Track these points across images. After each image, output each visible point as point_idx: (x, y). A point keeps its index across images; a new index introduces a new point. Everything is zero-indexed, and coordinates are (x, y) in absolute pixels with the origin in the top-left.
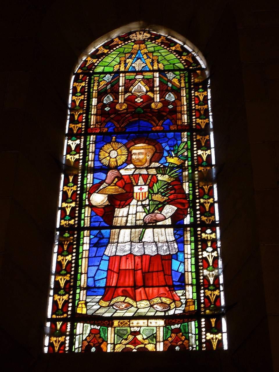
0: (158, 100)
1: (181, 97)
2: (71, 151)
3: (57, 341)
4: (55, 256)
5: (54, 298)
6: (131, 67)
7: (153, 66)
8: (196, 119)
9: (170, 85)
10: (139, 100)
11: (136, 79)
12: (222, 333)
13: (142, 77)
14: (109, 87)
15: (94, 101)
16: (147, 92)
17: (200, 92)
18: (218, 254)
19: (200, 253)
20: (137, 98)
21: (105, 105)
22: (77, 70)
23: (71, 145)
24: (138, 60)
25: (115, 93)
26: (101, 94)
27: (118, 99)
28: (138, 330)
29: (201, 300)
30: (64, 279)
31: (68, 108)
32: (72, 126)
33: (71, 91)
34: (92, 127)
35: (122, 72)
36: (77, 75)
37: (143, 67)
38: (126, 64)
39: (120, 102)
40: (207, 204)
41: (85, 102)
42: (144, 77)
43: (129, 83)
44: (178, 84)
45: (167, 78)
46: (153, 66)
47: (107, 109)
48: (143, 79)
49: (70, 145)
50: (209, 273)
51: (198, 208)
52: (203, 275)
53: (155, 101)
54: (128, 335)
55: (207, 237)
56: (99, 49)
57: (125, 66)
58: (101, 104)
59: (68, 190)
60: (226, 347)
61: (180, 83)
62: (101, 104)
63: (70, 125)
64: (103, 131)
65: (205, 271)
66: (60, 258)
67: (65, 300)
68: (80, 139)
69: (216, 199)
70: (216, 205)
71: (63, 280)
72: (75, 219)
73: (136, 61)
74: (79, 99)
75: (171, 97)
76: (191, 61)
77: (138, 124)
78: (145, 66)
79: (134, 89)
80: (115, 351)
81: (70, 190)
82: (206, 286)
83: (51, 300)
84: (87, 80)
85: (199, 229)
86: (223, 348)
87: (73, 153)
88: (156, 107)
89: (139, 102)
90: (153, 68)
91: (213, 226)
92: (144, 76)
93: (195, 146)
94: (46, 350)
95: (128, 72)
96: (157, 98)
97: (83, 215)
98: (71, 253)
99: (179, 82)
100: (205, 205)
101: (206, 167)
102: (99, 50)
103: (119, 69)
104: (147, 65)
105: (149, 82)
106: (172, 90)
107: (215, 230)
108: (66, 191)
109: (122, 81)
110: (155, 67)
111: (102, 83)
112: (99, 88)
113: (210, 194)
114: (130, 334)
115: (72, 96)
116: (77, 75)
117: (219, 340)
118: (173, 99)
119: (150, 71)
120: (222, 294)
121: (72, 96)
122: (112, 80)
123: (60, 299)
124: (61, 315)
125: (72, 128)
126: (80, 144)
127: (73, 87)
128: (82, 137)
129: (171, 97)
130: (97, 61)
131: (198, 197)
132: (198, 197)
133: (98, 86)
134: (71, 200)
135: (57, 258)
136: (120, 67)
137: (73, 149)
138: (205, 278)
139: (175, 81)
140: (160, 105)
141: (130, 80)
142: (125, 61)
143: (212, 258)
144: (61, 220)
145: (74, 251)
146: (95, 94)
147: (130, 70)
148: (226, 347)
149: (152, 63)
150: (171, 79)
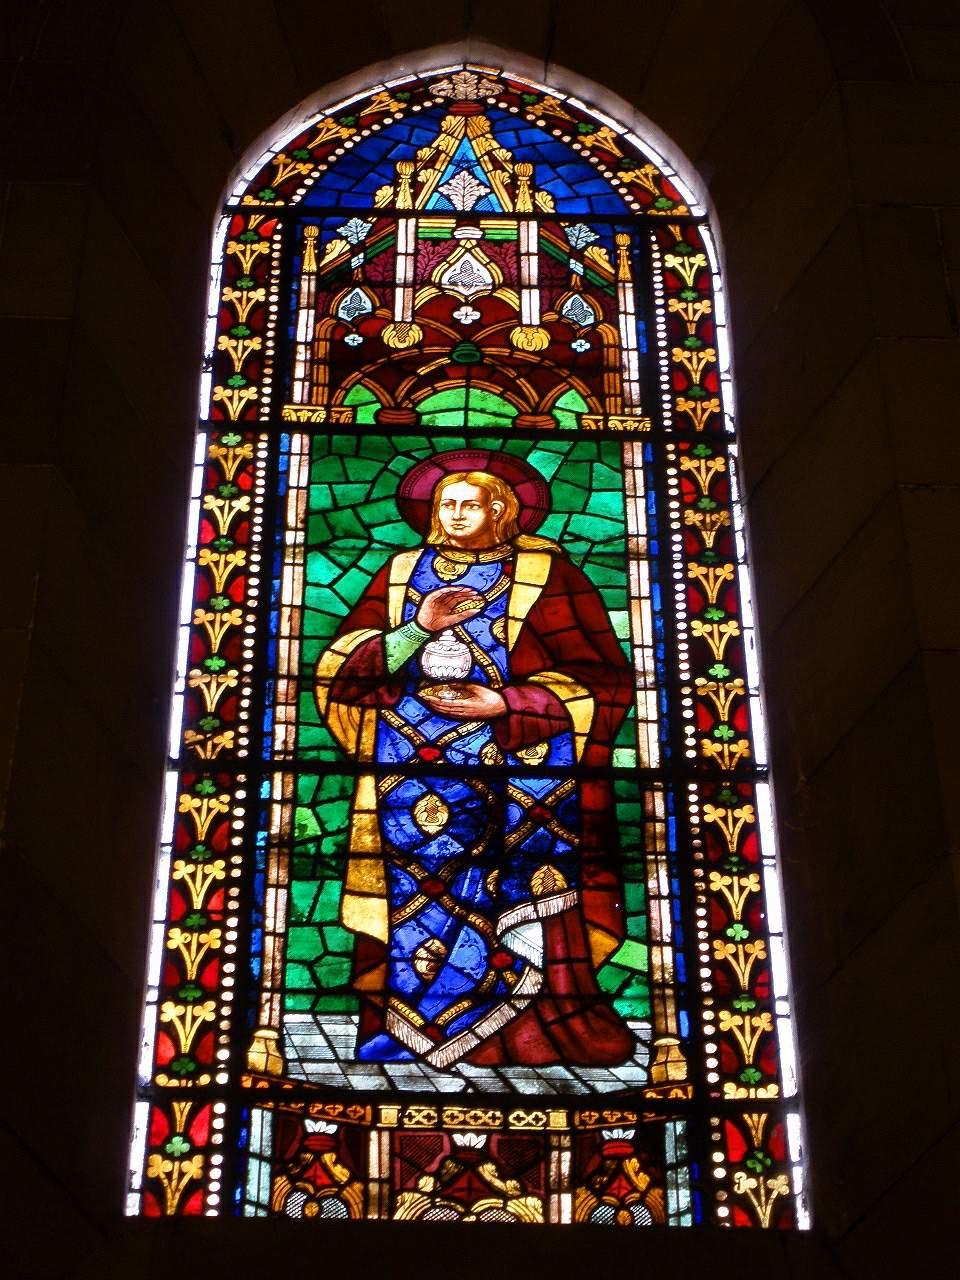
0: (536, 321)
2: (237, 324)
3: (175, 1175)
4: (157, 932)
5: (160, 1012)
6: (436, 195)
7: (513, 197)
8: (680, 510)
9: (576, 267)
10: (467, 315)
11: (457, 243)
12: (735, 563)
13: (478, 234)
14: (356, 262)
15: (305, 326)
16: (495, 287)
19: (704, 947)
20: (457, 309)
21: (342, 328)
22: (237, 192)
23: (218, 513)
25: (383, 288)
26: (335, 281)
27: (391, 306)
28: (479, 1146)
29: (686, 736)
30: (219, 685)
31: (201, 357)
32: (235, 248)
34: (250, 1210)
35: (407, 214)
37: (480, 198)
39: (398, 318)
42: (484, 235)
43: (434, 250)
44: (607, 266)
45: (567, 242)
46: (513, 197)
47: (353, 340)
48: (482, 243)
50: (701, 518)
51: (688, 714)
52: (707, 892)
53: (526, 320)
56: (320, 126)
58: (329, 322)
61: (616, 267)
62: (329, 322)
63: (225, 290)
64: (338, 419)
66: (231, 295)
67: (192, 1180)
68: (255, 441)
69: (790, 1087)
70: (794, 1123)
71: (214, 685)
72: (235, 729)
73: (453, 177)
74: (235, 457)
75: (577, 308)
78: (487, 194)
79: (444, 275)
81: (248, 253)
82: (680, 387)
83: (194, 508)
85: (671, 447)
87: (237, 381)
88: (529, 343)
89: (468, 321)
90: (514, 204)
91: (714, 438)
92: (482, 229)
93: (702, 924)
94: (133, 1206)
95: (425, 213)
96: (530, 305)
98: (234, 724)
99: (609, 262)
102: (321, 130)
103: (393, 202)
104: (492, 191)
105: (503, 253)
106: (587, 288)
107: (734, 611)
109: (405, 241)
110: (524, 205)
112: (323, 263)
113: (739, 722)
116: (241, 212)
118: (590, 320)
119: (504, 216)
120: (745, 576)
122: (367, 237)
123: (182, 1018)
125: (158, 1178)
126: (251, 515)
127: (226, 257)
128: (264, 437)
129: (577, 308)
130: (312, 170)
133: (319, 257)
134: (198, 994)
135: (173, 870)
136: (396, 194)
137: (243, 316)
140: (541, 340)
141: (436, 242)
142: (415, 175)
143: (746, 962)
145: (237, 841)
146: (307, 286)
147: (430, 207)
149: (512, 189)
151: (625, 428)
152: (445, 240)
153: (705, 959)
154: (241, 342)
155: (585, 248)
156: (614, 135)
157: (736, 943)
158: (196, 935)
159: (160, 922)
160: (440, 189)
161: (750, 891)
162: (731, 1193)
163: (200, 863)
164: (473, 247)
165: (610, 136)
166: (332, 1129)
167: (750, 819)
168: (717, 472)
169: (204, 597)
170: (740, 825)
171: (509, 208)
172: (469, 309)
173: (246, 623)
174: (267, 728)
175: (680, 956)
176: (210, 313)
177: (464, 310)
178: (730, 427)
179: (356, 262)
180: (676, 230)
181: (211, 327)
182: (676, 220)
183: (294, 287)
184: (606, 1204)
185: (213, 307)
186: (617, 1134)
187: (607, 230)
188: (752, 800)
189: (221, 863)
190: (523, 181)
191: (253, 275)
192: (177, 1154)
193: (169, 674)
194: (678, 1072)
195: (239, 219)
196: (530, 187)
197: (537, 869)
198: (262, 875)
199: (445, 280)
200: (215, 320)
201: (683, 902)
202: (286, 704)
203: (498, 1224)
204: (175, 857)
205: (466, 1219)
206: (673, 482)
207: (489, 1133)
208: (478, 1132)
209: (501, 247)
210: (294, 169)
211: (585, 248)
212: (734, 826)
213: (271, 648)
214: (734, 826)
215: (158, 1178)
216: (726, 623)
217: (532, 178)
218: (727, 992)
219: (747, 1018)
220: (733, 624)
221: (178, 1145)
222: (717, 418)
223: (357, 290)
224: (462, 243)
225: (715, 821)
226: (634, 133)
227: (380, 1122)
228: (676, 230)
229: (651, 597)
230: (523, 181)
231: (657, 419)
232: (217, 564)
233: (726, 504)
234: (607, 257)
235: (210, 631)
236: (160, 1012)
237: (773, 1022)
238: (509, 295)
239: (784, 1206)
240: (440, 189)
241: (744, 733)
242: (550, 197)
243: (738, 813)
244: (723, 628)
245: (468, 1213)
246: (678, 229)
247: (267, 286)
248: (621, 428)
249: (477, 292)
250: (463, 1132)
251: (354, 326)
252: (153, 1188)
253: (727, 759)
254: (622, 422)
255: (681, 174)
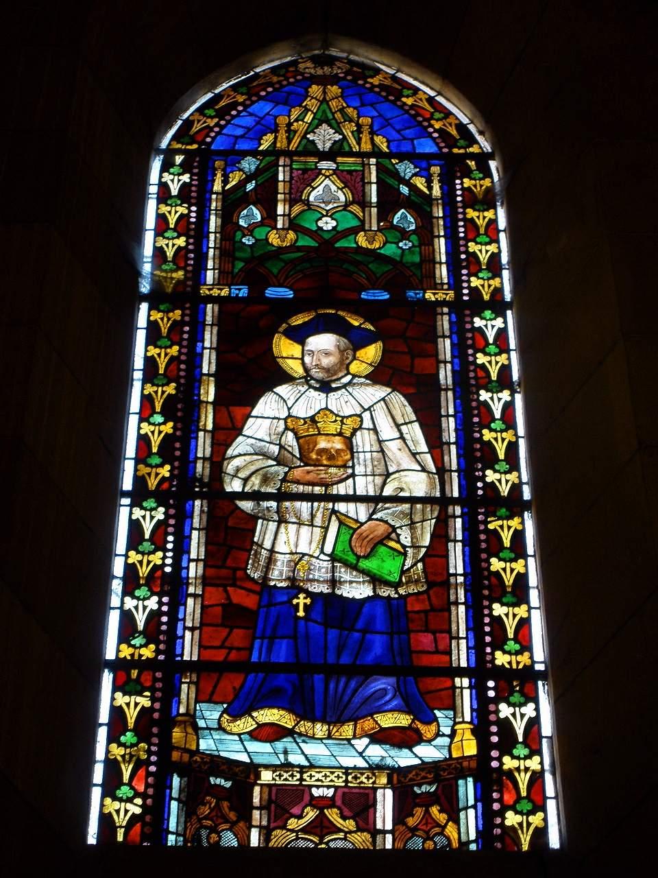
0: (375, 228)
1: (450, 604)
14: (250, 187)
17: (482, 278)
18: (541, 763)
23: (170, 183)
24: (321, 125)
26: (234, 202)
28: (330, 795)
33: (98, 775)
36: (169, 154)
38: (292, 133)
40: (522, 774)
41: (164, 619)
44: (425, 190)
46: (359, 142)
48: (335, 172)
49: (161, 247)
54: (305, 807)
55: (510, 663)
57: (288, 138)
59: (149, 474)
60: (554, 841)
61: (430, 188)
63: (152, 313)
65: (496, 606)
66: (153, 351)
73: (317, 128)
76: (454, 132)
77: (318, 678)
80: (271, 845)
82: (473, 270)
84: (170, 546)
86: (522, 496)
87: (147, 546)
97: (180, 625)
100: (516, 774)
101: (496, 356)
105: (353, 181)
106: (408, 204)
108: (147, 434)
110: (366, 147)
111: (235, 179)
114: (310, 804)
115: (103, 796)
117: (510, 442)
120: (519, 399)
121: (155, 238)
124: (188, 144)
125: (121, 707)
131: (495, 788)
132: (495, 788)
137: (164, 331)
138: (475, 292)
139: (420, 183)
142: (290, 124)
144: (114, 691)
148: (554, 841)
150: (407, 178)
151: (437, 299)
152: (312, 170)
153: (461, 216)
154: (146, 556)
155: (411, 178)
156: (427, 97)
157: (501, 473)
158: (133, 697)
159: (114, 608)
160: (308, 136)
161: (518, 572)
162: (469, 286)
163: (160, 386)
164: (331, 175)
165: (424, 97)
166: (228, 784)
167: (493, 217)
168: (495, 288)
169: (152, 339)
170: (517, 619)
171: (356, 149)
172: (328, 219)
173: (190, 211)
174: (184, 564)
175: (467, 548)
176: (101, 721)
177: (325, 219)
178: (508, 296)
179: (250, 187)
180: (472, 164)
181: (117, 586)
182: (472, 156)
183: (196, 392)
184: (417, 836)
185: (139, 363)
186: (424, 788)
187: (424, 165)
188: (500, 276)
189: (155, 599)
190: (366, 129)
191: (180, 196)
192: (154, 464)
193: (109, 553)
194: (471, 748)
195: (122, 674)
196: (370, 133)
197: (370, 381)
198: (186, 571)
199: (312, 199)
200: (95, 781)
201: (475, 624)
202: (207, 402)
203: (343, 850)
204: (141, 420)
205: (319, 847)
206: (459, 192)
207: (336, 788)
208: (328, 787)
209: (352, 175)
210: (205, 122)
211: (411, 178)
212: (522, 720)
213: (203, 276)
214: (522, 720)
215: (110, 813)
216: (522, 654)
217: (371, 126)
218: (498, 591)
219: (486, 281)
220: (511, 432)
221: (124, 791)
222: (498, 291)
223: (251, 206)
224: (323, 171)
225: (484, 363)
226: (442, 95)
227: (260, 779)
228: (472, 164)
229: (467, 638)
230: (366, 129)
231: (459, 295)
232: (141, 562)
233: (540, 807)
234: (426, 184)
235: (169, 217)
236: (131, 513)
237: (529, 611)
238: (354, 208)
239: (541, 833)
240: (308, 136)
241: (526, 647)
242: (385, 140)
243: (524, 710)
244: (498, 358)
245: (321, 843)
246: (473, 163)
247: (165, 550)
248: (433, 299)
249: (334, 208)
250: (318, 787)
251: (249, 231)
252: (106, 821)
253: (479, 189)
254: (434, 294)
255: (475, 121)
